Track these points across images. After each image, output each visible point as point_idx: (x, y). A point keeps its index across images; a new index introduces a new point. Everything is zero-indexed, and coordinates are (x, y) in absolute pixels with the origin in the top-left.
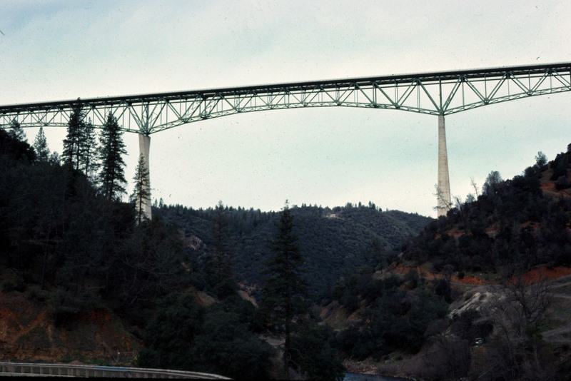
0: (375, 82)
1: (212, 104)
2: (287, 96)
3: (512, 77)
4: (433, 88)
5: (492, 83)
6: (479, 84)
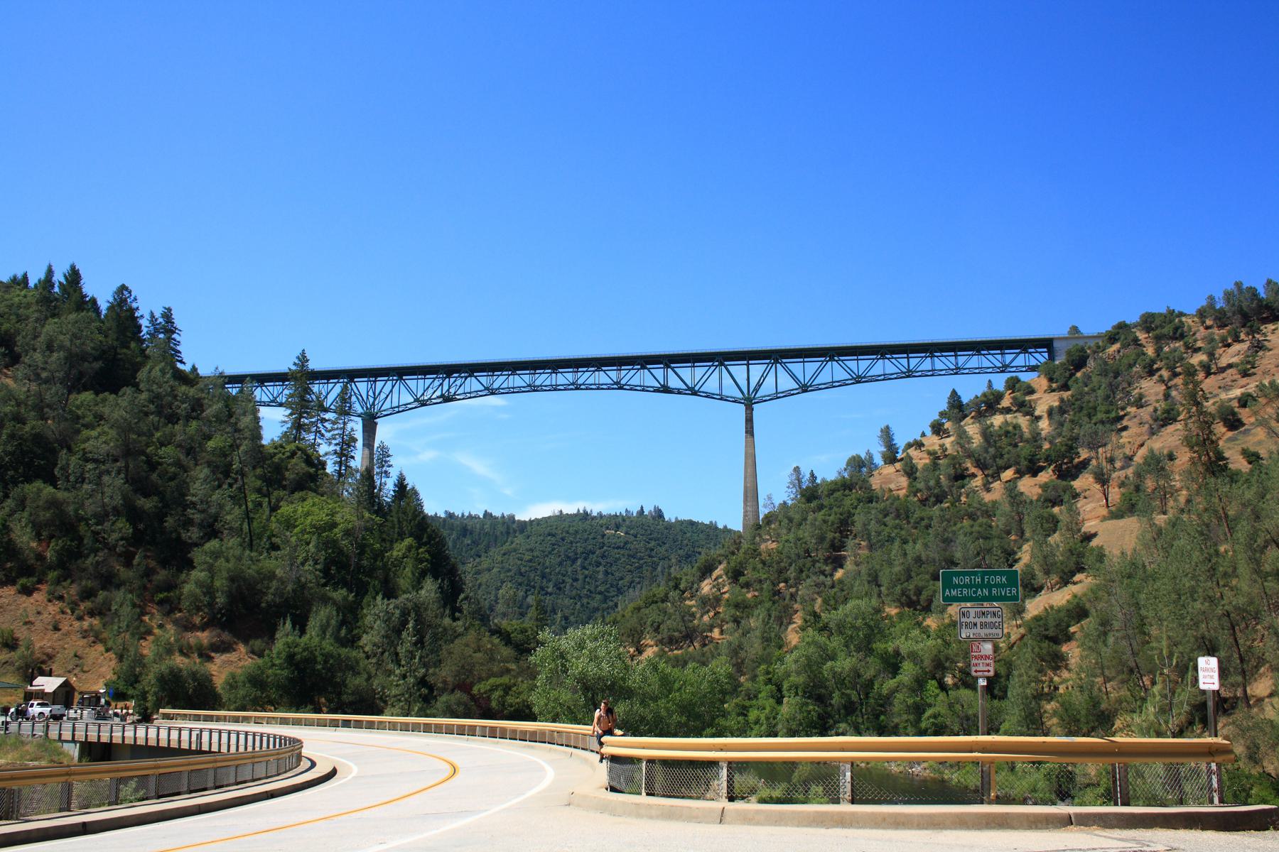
0: (669, 361)
1: (458, 383)
2: (554, 375)
3: (836, 358)
4: (739, 370)
5: (812, 366)
6: (796, 367)
